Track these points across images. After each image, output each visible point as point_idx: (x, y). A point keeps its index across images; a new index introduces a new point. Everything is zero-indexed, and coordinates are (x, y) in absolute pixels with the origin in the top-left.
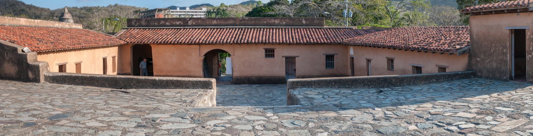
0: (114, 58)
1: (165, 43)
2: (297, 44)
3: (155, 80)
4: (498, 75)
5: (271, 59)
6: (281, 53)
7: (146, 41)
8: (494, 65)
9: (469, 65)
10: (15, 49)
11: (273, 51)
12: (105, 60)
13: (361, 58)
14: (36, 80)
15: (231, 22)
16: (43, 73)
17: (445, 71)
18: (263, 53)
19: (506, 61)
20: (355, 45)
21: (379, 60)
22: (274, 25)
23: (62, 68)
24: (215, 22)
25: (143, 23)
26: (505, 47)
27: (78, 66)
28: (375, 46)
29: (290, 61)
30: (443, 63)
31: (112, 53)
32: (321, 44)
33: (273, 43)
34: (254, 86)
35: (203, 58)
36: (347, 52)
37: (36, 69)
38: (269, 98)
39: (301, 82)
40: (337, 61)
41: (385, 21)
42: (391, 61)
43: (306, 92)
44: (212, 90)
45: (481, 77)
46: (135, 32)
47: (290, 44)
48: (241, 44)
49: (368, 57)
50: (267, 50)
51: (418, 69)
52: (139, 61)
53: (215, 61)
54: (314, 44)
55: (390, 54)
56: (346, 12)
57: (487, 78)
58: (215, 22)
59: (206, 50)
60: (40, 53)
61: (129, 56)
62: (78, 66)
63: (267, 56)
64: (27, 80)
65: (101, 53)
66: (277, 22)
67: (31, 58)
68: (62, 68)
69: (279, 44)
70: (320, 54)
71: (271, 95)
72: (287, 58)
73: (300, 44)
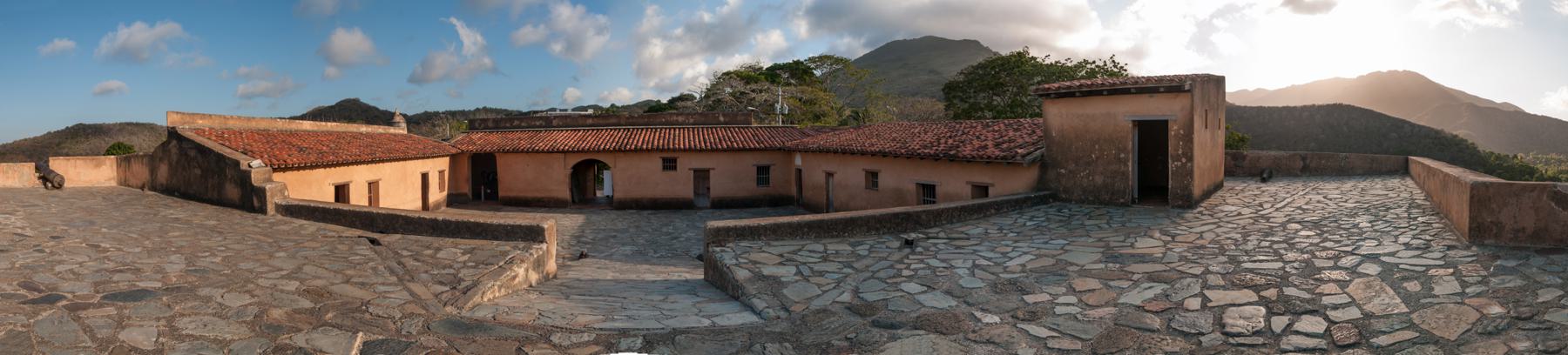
0: (441, 172)
1: (516, 151)
2: (712, 150)
3: (435, 220)
4: (1107, 197)
5: (672, 173)
6: (686, 164)
7: (488, 149)
8: (1099, 180)
9: (1041, 183)
10: (237, 163)
11: (674, 160)
12: (425, 177)
13: (815, 173)
14: (263, 210)
15: (613, 121)
16: (273, 200)
17: (987, 195)
18: (660, 163)
19: (1125, 174)
20: (806, 151)
21: (851, 175)
22: (677, 123)
23: (341, 192)
24: (590, 121)
25: (490, 124)
26: (1124, 150)
27: (373, 187)
28: (845, 153)
29: (701, 176)
30: (982, 177)
31: (437, 167)
32: (751, 150)
33: (674, 150)
34: (645, 213)
35: (569, 171)
36: (792, 161)
37: (261, 193)
38: (668, 234)
39: (735, 228)
40: (774, 174)
41: (829, 120)
42: (872, 177)
43: (755, 256)
44: (544, 246)
45: (1069, 201)
46: (476, 136)
47: (701, 150)
48: (625, 151)
49: (830, 169)
50: (664, 160)
51: (982, 190)
52: (479, 179)
53: (590, 176)
54: (739, 150)
55: (873, 165)
56: (778, 106)
57: (1082, 202)
58: (590, 121)
59: (574, 160)
60: (275, 170)
61: (465, 168)
62: (373, 187)
63: (665, 168)
64: (251, 209)
65: (416, 167)
66: (680, 119)
67: (256, 179)
68: (341, 192)
69: (685, 150)
70: (749, 163)
71: (670, 229)
72: (695, 171)
73: (717, 150)
